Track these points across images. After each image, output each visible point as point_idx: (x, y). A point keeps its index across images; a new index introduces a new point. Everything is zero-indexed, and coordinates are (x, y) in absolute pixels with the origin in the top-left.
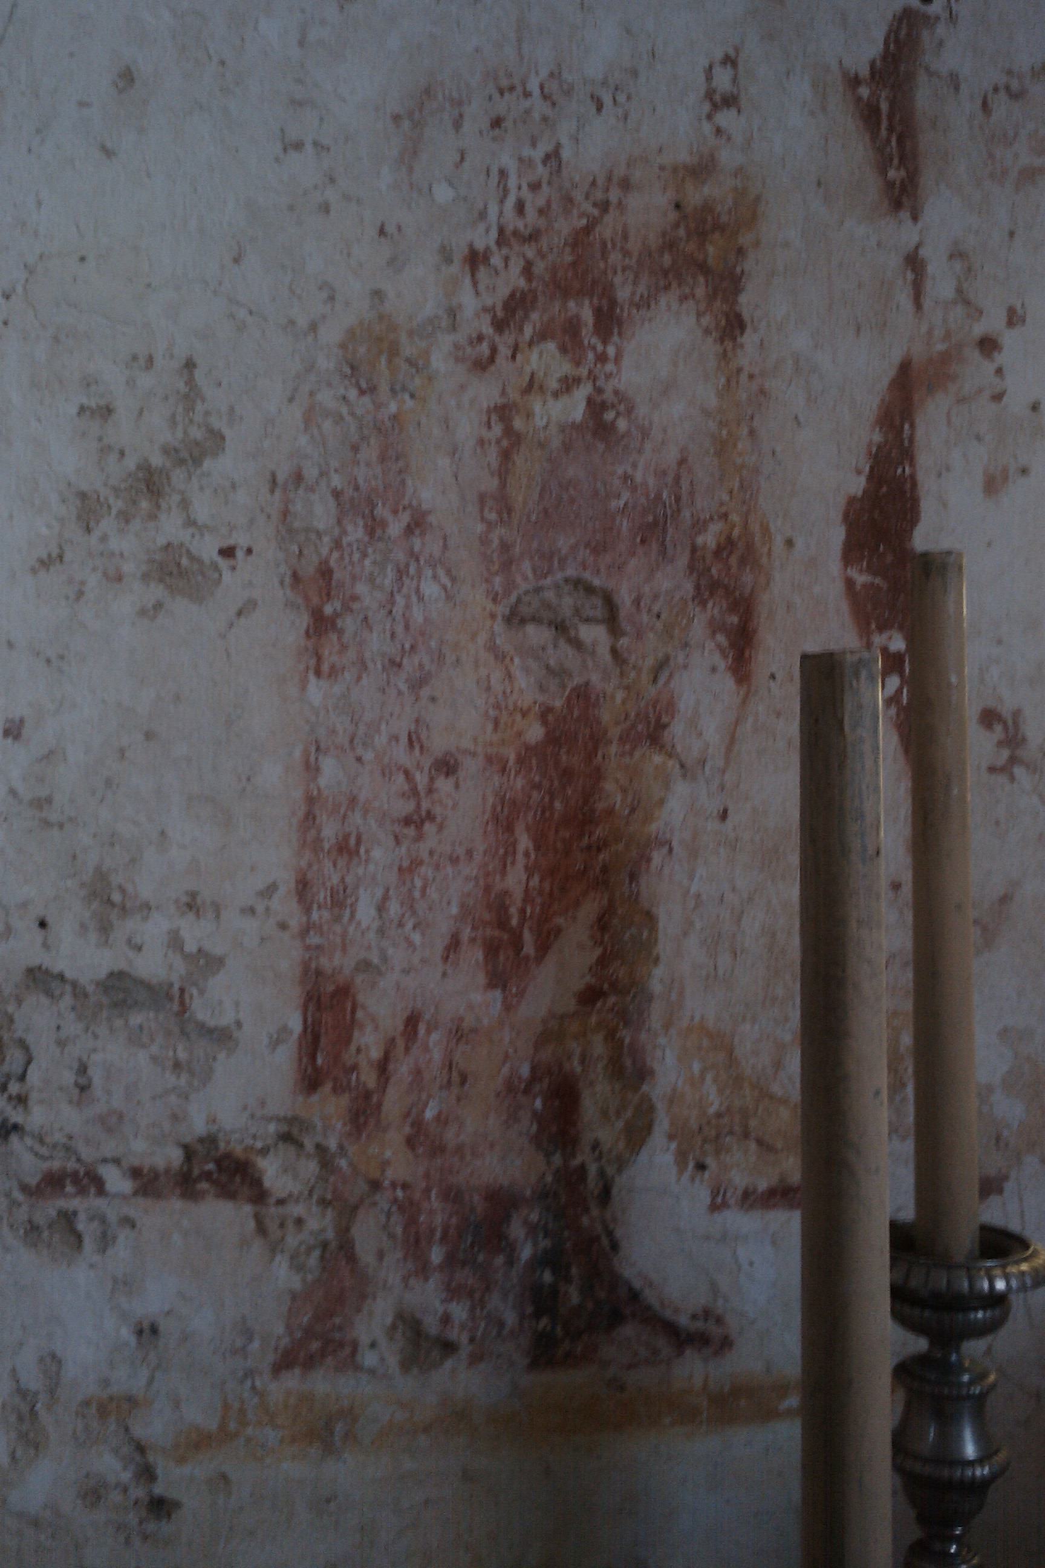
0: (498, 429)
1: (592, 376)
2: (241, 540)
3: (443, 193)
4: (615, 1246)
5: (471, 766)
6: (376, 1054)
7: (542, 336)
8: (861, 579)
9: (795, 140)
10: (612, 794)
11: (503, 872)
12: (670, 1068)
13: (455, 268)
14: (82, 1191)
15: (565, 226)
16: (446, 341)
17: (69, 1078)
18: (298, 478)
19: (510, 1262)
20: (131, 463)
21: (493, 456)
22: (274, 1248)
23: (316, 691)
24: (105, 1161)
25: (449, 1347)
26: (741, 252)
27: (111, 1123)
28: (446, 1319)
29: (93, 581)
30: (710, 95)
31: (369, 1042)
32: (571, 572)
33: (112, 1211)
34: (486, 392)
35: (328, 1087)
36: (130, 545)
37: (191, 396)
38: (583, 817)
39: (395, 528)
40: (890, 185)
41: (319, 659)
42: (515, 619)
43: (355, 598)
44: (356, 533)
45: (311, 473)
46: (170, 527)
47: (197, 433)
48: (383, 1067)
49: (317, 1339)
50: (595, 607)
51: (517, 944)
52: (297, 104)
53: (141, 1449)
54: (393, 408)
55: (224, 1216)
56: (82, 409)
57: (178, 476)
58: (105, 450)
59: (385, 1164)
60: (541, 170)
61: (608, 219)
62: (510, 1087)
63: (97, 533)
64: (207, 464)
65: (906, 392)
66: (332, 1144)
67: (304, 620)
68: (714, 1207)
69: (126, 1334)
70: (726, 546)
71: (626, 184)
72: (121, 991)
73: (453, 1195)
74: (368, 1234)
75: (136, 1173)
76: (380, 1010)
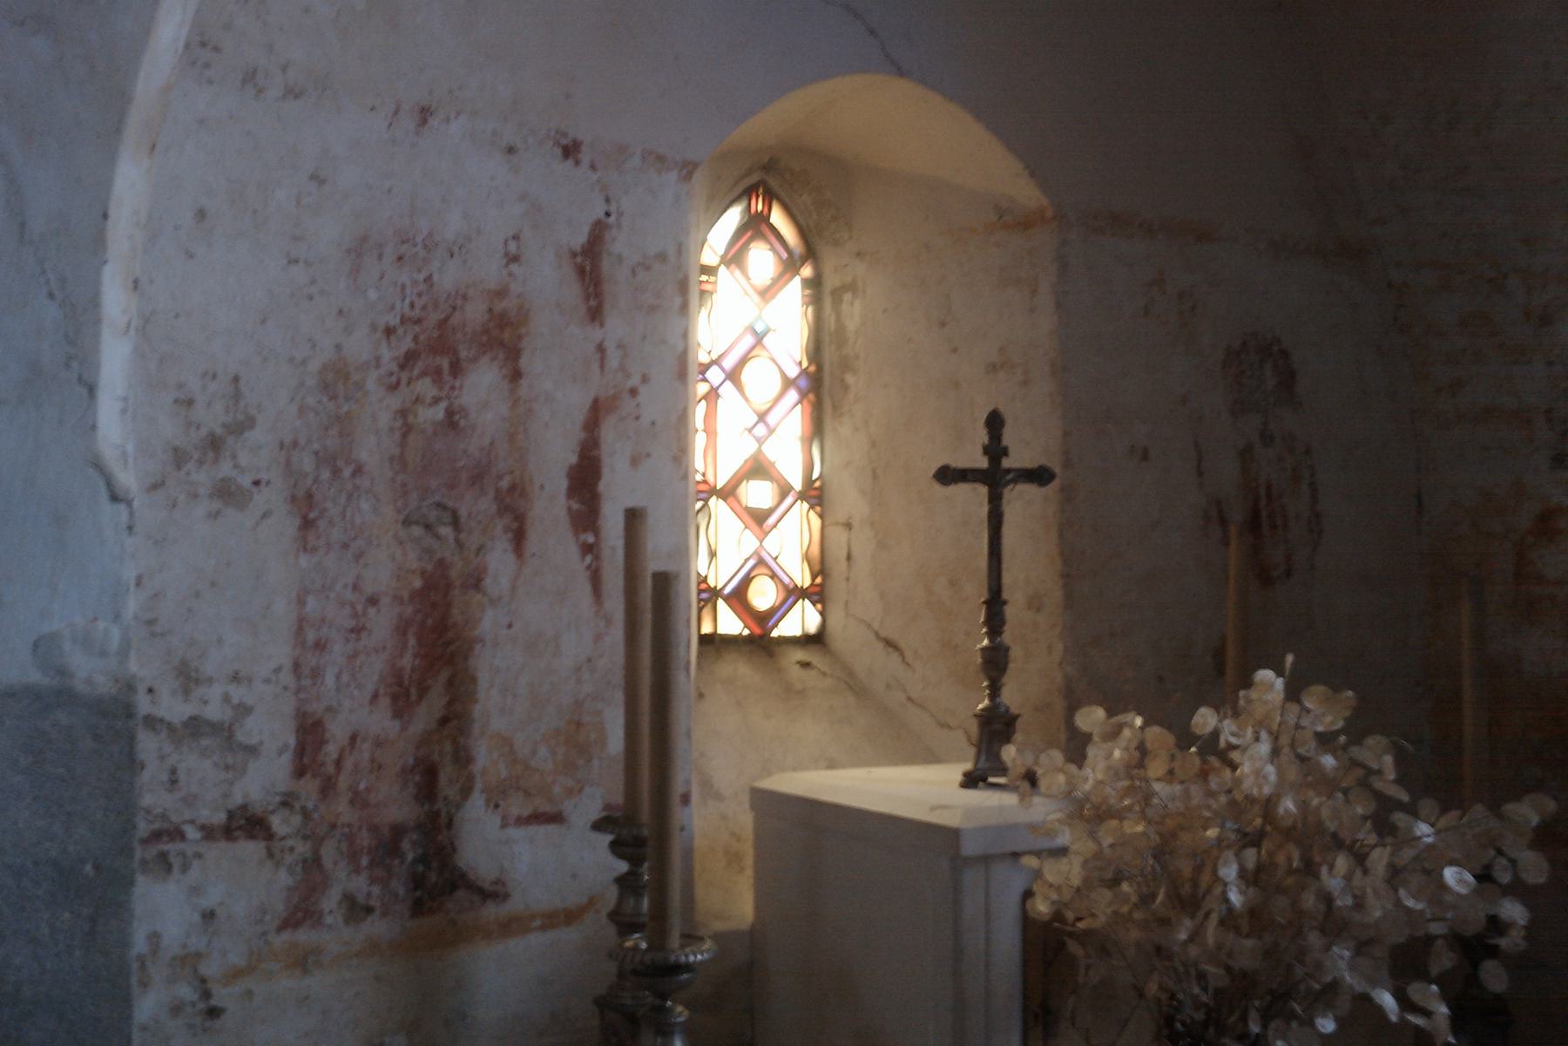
0: (399, 423)
1: (448, 397)
2: (264, 476)
3: (372, 295)
4: (454, 850)
5: (385, 601)
6: (335, 756)
7: (424, 374)
8: (576, 506)
9: (546, 282)
10: (456, 615)
11: (401, 656)
12: (484, 756)
13: (378, 335)
14: (172, 840)
15: (434, 317)
16: (373, 376)
17: (165, 777)
18: (295, 444)
19: (402, 862)
20: (204, 431)
21: (397, 435)
22: (278, 864)
23: (304, 561)
24: (185, 822)
25: (369, 910)
26: (520, 337)
27: (190, 801)
28: (369, 895)
29: (182, 497)
30: (506, 254)
31: (331, 750)
32: (437, 498)
33: (190, 850)
34: (395, 402)
35: (308, 775)
36: (203, 478)
37: (237, 396)
38: (442, 627)
39: (347, 473)
40: (589, 309)
41: (306, 542)
42: (407, 523)
43: (325, 510)
44: (326, 474)
45: (302, 442)
46: (225, 469)
47: (240, 417)
48: (338, 763)
49: (301, 913)
50: (447, 517)
51: (408, 694)
52: (296, 239)
53: (203, 981)
54: (346, 408)
55: (250, 849)
56: (176, 401)
57: (230, 440)
58: (189, 424)
59: (338, 816)
60: (422, 287)
61: (457, 314)
62: (404, 771)
63: (185, 470)
64: (246, 434)
65: (596, 414)
66: (310, 805)
67: (298, 521)
68: (504, 826)
69: (196, 917)
70: (513, 488)
71: (465, 297)
72: (195, 727)
73: (374, 829)
74: (328, 853)
75: (203, 828)
76: (337, 731)
